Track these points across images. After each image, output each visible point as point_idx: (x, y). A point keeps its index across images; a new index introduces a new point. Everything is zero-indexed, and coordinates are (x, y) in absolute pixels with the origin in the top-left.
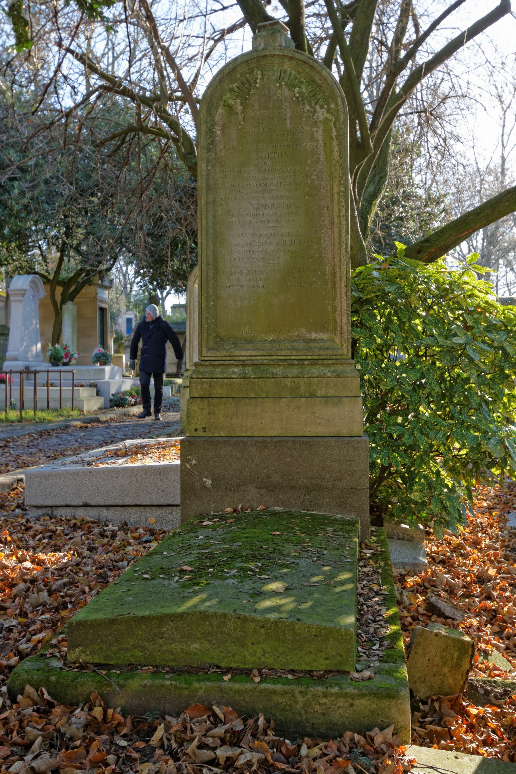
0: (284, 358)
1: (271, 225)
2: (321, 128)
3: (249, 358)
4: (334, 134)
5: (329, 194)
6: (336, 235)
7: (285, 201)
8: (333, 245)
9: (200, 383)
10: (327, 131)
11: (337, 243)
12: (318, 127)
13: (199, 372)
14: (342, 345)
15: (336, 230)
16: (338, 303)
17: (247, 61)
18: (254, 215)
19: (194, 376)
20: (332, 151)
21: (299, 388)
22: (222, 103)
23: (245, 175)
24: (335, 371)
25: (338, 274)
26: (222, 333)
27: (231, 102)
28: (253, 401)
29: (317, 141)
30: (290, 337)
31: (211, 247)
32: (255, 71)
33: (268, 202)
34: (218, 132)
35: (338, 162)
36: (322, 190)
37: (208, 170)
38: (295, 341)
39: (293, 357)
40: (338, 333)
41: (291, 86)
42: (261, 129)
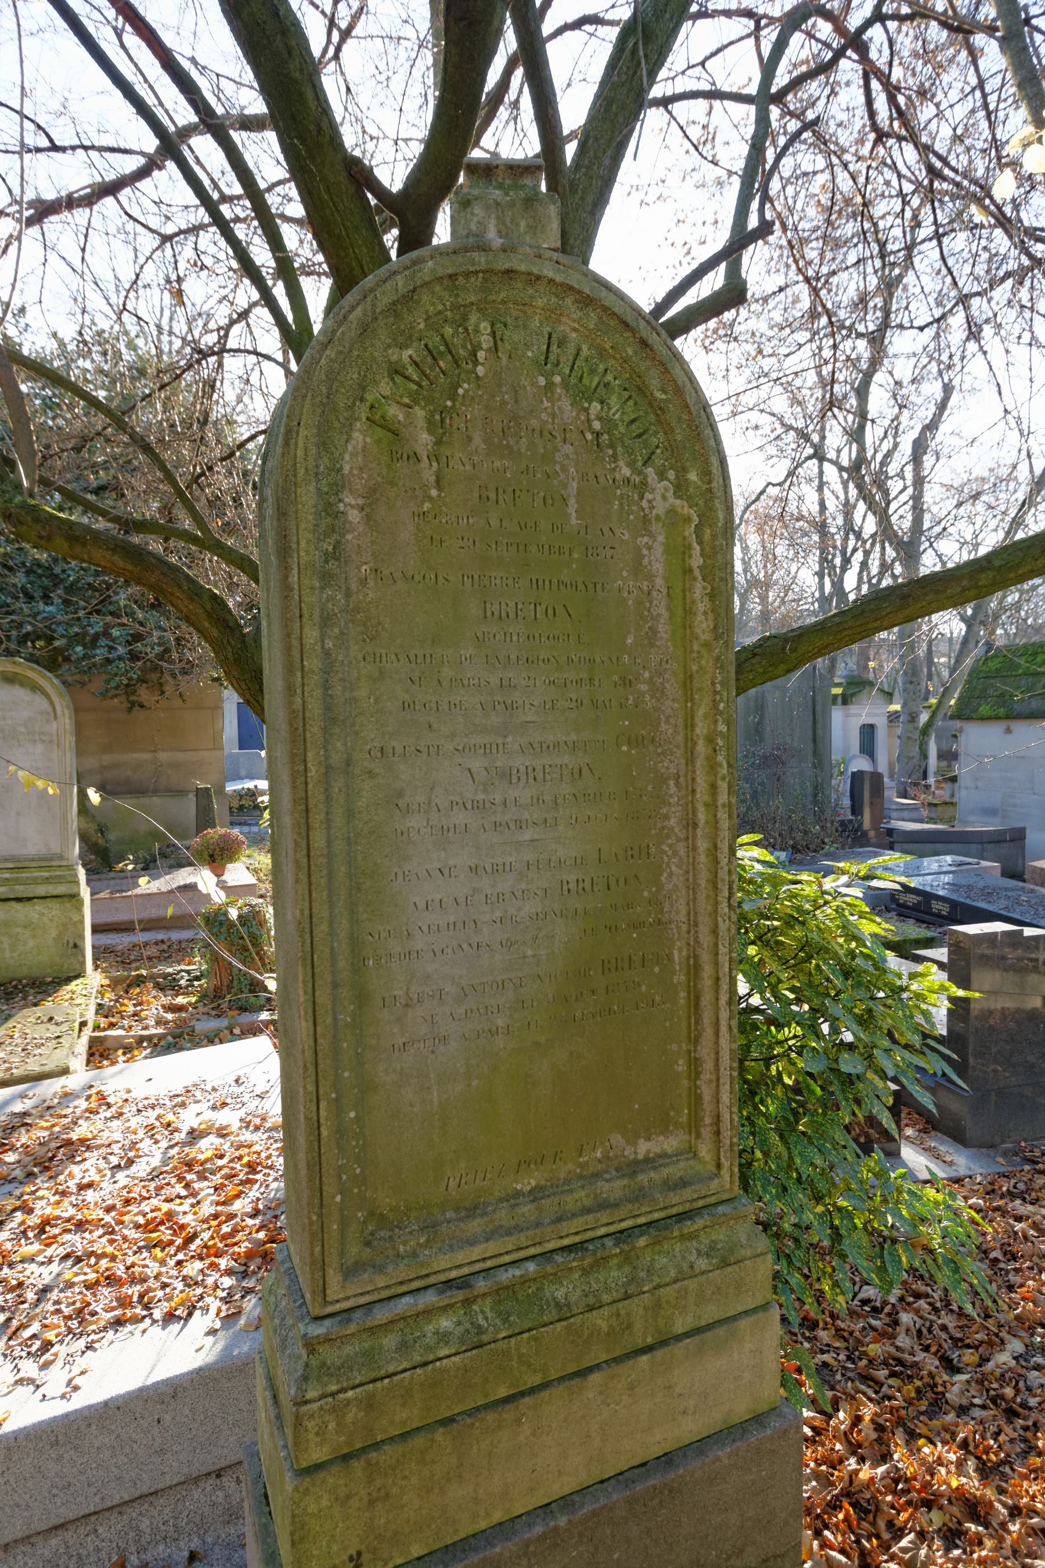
0: (577, 1239)
1: (527, 835)
2: (661, 538)
3: (478, 1267)
4: (697, 561)
5: (680, 739)
6: (703, 858)
7: (566, 759)
8: (693, 888)
9: (333, 1410)
10: (679, 552)
11: (703, 883)
12: (651, 535)
13: (326, 1371)
14: (719, 1166)
15: (703, 845)
16: (705, 1051)
17: (452, 277)
18: (478, 807)
19: (311, 1394)
20: (689, 612)
21: (629, 1326)
22: (363, 412)
23: (447, 672)
24: (713, 1247)
25: (707, 971)
26: (385, 1201)
27: (394, 412)
28: (509, 1413)
29: (650, 577)
30: (583, 1166)
31: (343, 926)
32: (473, 319)
33: (520, 762)
34: (354, 516)
35: (706, 645)
36: (663, 727)
37: (327, 653)
38: (597, 1175)
39: (602, 1231)
40: (706, 1132)
41: (581, 395)
42: (495, 522)
